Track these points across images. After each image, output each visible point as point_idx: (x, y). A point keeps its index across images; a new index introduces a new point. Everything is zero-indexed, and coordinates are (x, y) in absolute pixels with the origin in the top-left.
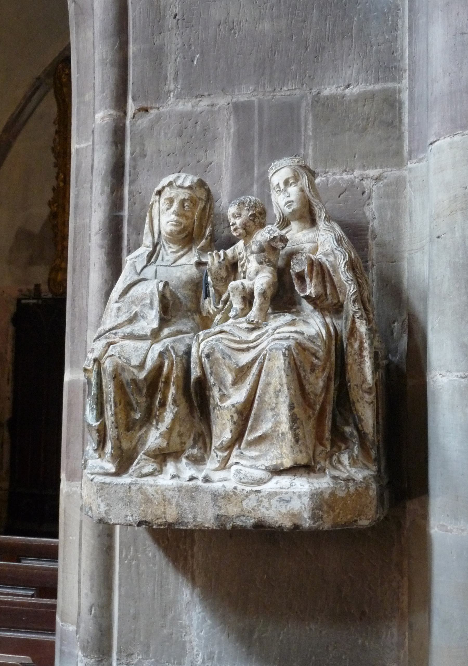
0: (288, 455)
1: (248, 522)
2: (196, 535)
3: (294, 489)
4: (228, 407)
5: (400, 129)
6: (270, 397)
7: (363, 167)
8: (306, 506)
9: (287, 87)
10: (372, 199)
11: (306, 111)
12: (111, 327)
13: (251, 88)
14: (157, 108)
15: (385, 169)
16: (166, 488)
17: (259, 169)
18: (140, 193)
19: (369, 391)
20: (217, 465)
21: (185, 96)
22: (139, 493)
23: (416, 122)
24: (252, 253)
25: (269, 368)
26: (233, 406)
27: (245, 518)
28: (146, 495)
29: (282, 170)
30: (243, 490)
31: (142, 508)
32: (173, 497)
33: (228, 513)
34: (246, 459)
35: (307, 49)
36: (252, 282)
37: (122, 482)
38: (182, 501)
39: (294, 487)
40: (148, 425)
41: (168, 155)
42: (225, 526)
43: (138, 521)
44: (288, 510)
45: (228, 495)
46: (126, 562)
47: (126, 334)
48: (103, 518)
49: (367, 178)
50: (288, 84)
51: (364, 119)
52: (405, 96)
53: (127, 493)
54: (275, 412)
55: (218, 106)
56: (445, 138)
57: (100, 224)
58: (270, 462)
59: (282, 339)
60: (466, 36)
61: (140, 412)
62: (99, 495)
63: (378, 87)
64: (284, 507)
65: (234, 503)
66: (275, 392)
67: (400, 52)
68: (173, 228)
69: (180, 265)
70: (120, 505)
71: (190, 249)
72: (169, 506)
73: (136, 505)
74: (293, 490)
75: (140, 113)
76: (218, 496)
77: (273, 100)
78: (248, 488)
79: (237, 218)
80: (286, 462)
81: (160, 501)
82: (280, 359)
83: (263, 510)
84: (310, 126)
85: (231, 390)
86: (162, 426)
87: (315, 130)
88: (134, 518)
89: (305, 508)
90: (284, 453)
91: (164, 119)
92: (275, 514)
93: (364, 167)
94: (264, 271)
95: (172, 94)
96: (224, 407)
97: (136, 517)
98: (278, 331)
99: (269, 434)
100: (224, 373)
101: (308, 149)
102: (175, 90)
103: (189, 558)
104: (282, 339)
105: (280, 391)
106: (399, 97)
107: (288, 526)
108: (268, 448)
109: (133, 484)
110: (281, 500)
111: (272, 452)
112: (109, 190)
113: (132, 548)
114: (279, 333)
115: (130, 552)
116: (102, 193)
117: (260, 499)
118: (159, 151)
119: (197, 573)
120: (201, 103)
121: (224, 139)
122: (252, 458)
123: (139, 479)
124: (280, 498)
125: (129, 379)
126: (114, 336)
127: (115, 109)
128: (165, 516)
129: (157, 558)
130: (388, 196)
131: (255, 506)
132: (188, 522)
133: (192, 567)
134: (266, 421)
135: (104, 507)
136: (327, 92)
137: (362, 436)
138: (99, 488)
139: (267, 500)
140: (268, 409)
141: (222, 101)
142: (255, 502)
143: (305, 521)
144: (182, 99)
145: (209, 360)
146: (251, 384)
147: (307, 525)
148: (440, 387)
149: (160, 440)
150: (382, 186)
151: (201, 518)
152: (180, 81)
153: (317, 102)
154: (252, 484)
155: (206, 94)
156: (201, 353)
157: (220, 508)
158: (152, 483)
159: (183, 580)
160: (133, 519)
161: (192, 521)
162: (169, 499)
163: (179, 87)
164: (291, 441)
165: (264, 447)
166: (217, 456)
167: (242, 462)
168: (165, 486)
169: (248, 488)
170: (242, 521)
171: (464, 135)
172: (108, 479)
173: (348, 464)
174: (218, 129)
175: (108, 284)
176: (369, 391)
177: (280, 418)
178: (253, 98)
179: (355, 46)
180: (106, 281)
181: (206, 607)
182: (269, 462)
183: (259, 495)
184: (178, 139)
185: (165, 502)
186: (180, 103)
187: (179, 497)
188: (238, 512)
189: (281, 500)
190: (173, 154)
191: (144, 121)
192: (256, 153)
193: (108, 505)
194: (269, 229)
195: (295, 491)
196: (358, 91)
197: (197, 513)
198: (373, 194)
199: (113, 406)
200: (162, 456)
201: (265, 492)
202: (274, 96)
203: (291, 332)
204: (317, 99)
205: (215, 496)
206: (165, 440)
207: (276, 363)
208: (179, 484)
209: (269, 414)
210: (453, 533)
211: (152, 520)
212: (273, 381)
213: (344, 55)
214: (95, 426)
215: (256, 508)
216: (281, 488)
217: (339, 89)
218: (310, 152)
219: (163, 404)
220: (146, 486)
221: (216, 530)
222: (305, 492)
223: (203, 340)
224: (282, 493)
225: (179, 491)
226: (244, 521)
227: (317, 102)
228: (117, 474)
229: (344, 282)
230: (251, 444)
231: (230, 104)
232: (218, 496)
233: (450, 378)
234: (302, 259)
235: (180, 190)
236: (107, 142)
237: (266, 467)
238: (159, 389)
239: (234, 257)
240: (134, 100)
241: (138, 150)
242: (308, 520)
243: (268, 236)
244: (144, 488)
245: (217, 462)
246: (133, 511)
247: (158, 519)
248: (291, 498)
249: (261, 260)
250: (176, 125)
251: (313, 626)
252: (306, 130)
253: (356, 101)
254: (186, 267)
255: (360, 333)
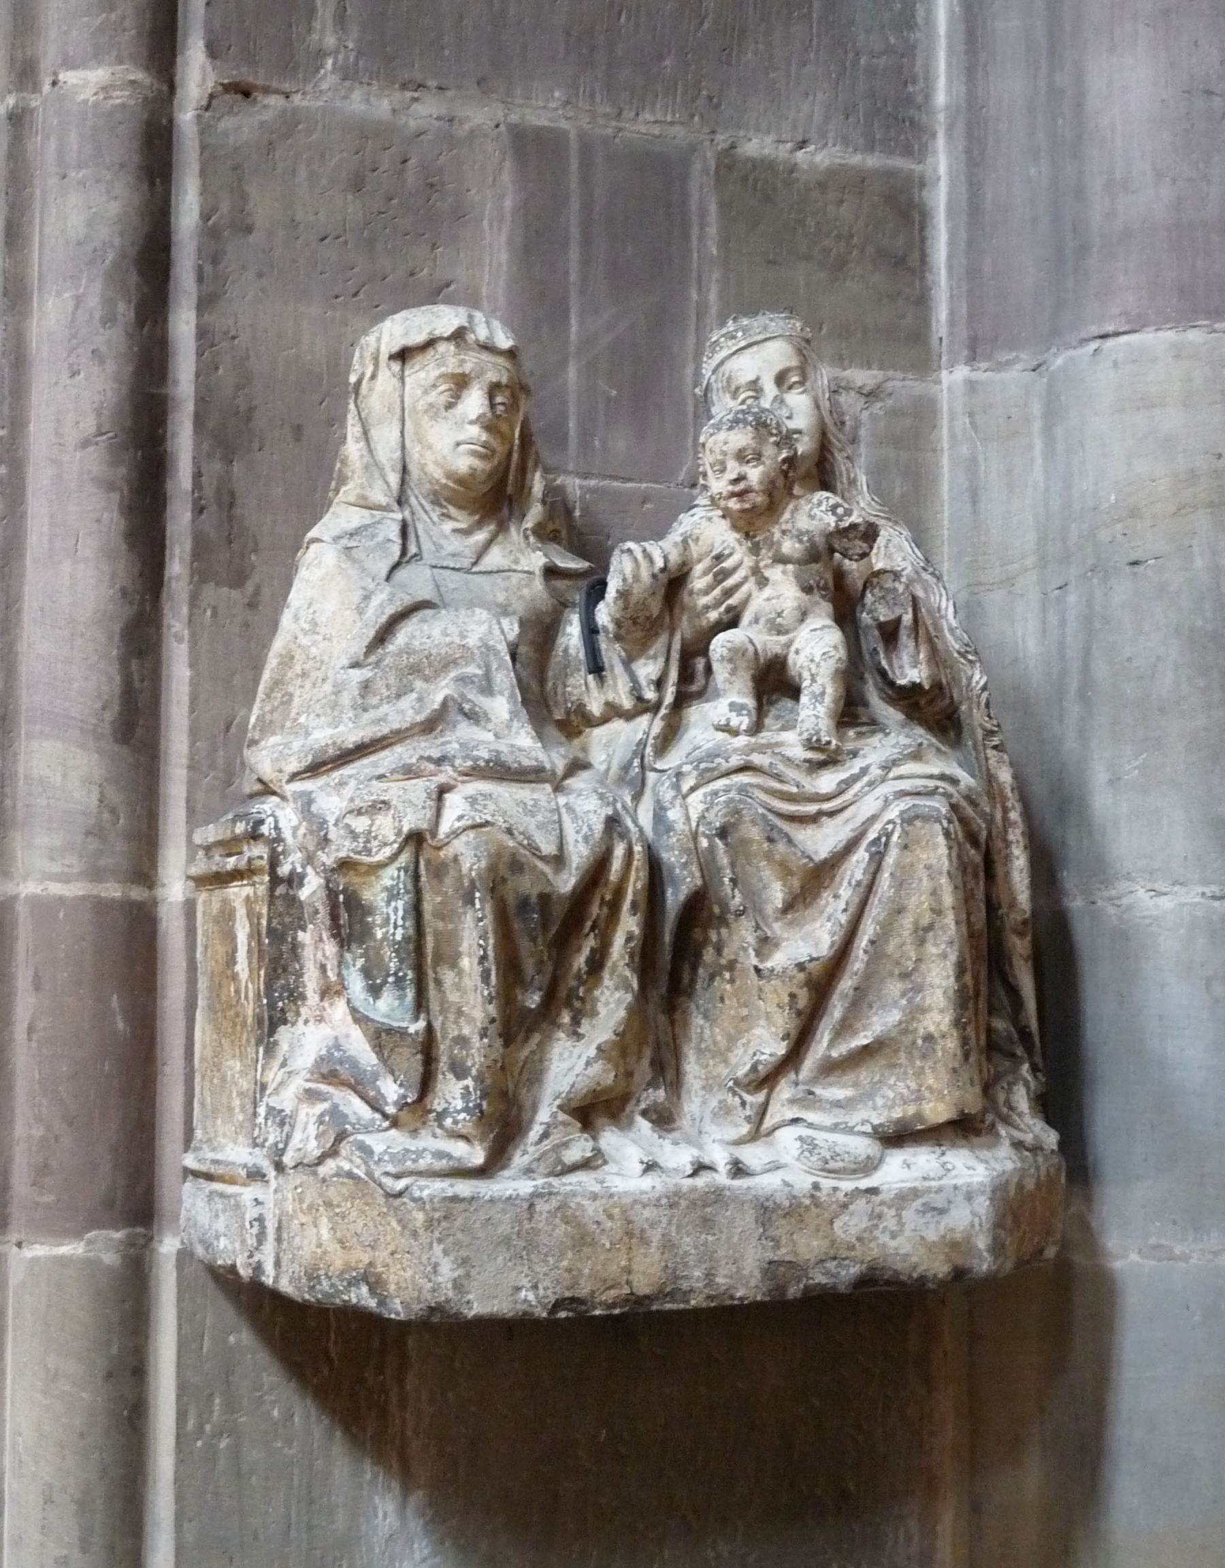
0: (940, 1092)
1: (843, 1273)
2: (411, 1342)
3: (956, 1176)
4: (785, 970)
5: (923, 278)
6: (902, 941)
7: (840, 360)
8: (984, 1218)
9: (653, 112)
10: (859, 442)
11: (701, 188)
12: (366, 740)
13: (557, 94)
14: (283, 93)
15: (890, 373)
16: (635, 1201)
17: (581, 323)
18: (234, 338)
19: (1021, 928)
20: (745, 1129)
21: (371, 78)
22: (557, 1221)
23: (987, 269)
24: (781, 560)
25: (904, 867)
26: (801, 967)
27: (835, 1263)
28: (579, 1225)
29: (768, 344)
30: (835, 1189)
31: (565, 1263)
32: (653, 1225)
33: (796, 1254)
34: (823, 1109)
35: (701, 24)
36: (783, 639)
37: (508, 1193)
38: (678, 1233)
39: (953, 1173)
40: (544, 1026)
41: (323, 239)
42: (781, 1289)
43: (553, 1299)
44: (942, 1233)
45: (800, 1205)
46: (199, 1443)
47: (482, 764)
48: (448, 1301)
49: (847, 389)
50: (653, 105)
51: (839, 237)
52: (940, 199)
53: (520, 1223)
54: (912, 982)
55: (467, 127)
56: (1158, 330)
57: (99, 415)
58: (886, 1113)
59: (918, 794)
60: (1217, 101)
61: (540, 989)
62: (437, 1234)
63: (873, 161)
64: (932, 1226)
65: (812, 1227)
66: (916, 931)
67: (921, 84)
68: (477, 463)
69: (498, 572)
70: (500, 1259)
71: (502, 528)
72: (642, 1251)
73: (546, 1255)
74: (954, 1182)
75: (227, 97)
76: (774, 1210)
77: (617, 140)
78: (847, 1185)
79: (748, 462)
80: (934, 1110)
81: (618, 1237)
82: (935, 846)
83: (884, 1239)
84: (713, 230)
85: (777, 927)
86: (593, 1027)
87: (724, 242)
88: (541, 1292)
89: (980, 1225)
90: (930, 1088)
91: (309, 132)
92: (910, 1246)
93: (841, 359)
94: (817, 610)
95: (330, 62)
96: (773, 970)
97: (546, 1289)
98: (895, 772)
99: (892, 1039)
100: (761, 880)
101: (709, 290)
102: (337, 52)
103: (393, 1408)
104: (918, 794)
105: (930, 928)
106: (920, 197)
107: (940, 1276)
108: (877, 1078)
109: (541, 1195)
110: (928, 1209)
111: (890, 1087)
112: (132, 314)
113: (217, 1401)
114: (900, 777)
115: (211, 1412)
116: (109, 319)
117: (877, 1210)
118: (293, 224)
119: (415, 1446)
120: (416, 107)
121: (485, 224)
122: (837, 1104)
123: (554, 1181)
124: (924, 1204)
125: (534, 893)
126: (432, 767)
127: (147, 68)
128: (631, 1278)
129: (296, 1419)
130: (896, 441)
131: (865, 1230)
132: (691, 1291)
133: (403, 1433)
134: (883, 1007)
135: (452, 1270)
136: (755, 146)
137: (1024, 1034)
138: (437, 1215)
139: (893, 1212)
140: (891, 974)
141: (480, 115)
142: (865, 1219)
143: (980, 1257)
144: (361, 83)
145: (726, 845)
146: (851, 910)
147: (985, 1267)
148: (1148, 921)
149: (597, 1067)
150: (882, 413)
151: (726, 1276)
152: (355, 32)
153: (730, 168)
154: (854, 1172)
155: (432, 83)
156: (698, 826)
157: (777, 1244)
158: (596, 1188)
159: (375, 1476)
160: (537, 1297)
161: (700, 1285)
162: (643, 1231)
163: (351, 45)
164: (955, 1055)
165: (864, 1075)
166: (743, 1104)
167: (811, 1116)
168: (633, 1194)
169: (847, 1185)
170: (827, 1273)
171: (1214, 331)
172: (464, 1188)
173: (1027, 1111)
174: (468, 190)
175: (131, 603)
176: (1021, 928)
177: (923, 998)
178: (564, 125)
179: (819, 45)
180: (124, 592)
181: (442, 1543)
182: (878, 1114)
183: (876, 1199)
184: (350, 197)
185: (631, 1238)
186: (357, 95)
187: (670, 1223)
188: (823, 1250)
189: (928, 1209)
190: (337, 238)
191: (243, 125)
192: (573, 277)
193: (464, 1262)
194: (831, 502)
195: (960, 1182)
196: (827, 162)
197: (718, 1261)
198: (862, 432)
199: (493, 973)
200: (591, 1111)
201: (890, 1190)
202: (620, 130)
203: (931, 777)
204: (728, 162)
205: (767, 1211)
206: (609, 1066)
207: (925, 856)
208: (672, 1189)
209: (894, 988)
210: (1193, 1261)
211: (593, 1292)
212: (912, 902)
213: (794, 62)
214: (417, 1033)
215: (866, 1235)
216: (925, 1179)
217: (781, 147)
218: (713, 296)
219: (597, 964)
220: (578, 1199)
221: (762, 1303)
222: (982, 1184)
223: (693, 789)
224: (928, 1190)
225: (671, 1206)
226: (834, 1271)
227: (730, 168)
228: (482, 1172)
229: (956, 655)
230: (830, 1068)
231: (502, 128)
232: (774, 1210)
233: (1183, 900)
234: (895, 589)
235: (485, 356)
236: (122, 166)
237: (874, 1128)
238: (589, 924)
239: (684, 564)
240: (213, 51)
241: (225, 207)
242: (985, 1254)
243: (831, 520)
244: (573, 1205)
245: (741, 1121)
246: (537, 1273)
247: (610, 1288)
248: (950, 1202)
249: (811, 582)
250: (345, 154)
251: (724, 1548)
252: (701, 239)
253: (822, 186)
254: (515, 578)
255: (999, 785)
